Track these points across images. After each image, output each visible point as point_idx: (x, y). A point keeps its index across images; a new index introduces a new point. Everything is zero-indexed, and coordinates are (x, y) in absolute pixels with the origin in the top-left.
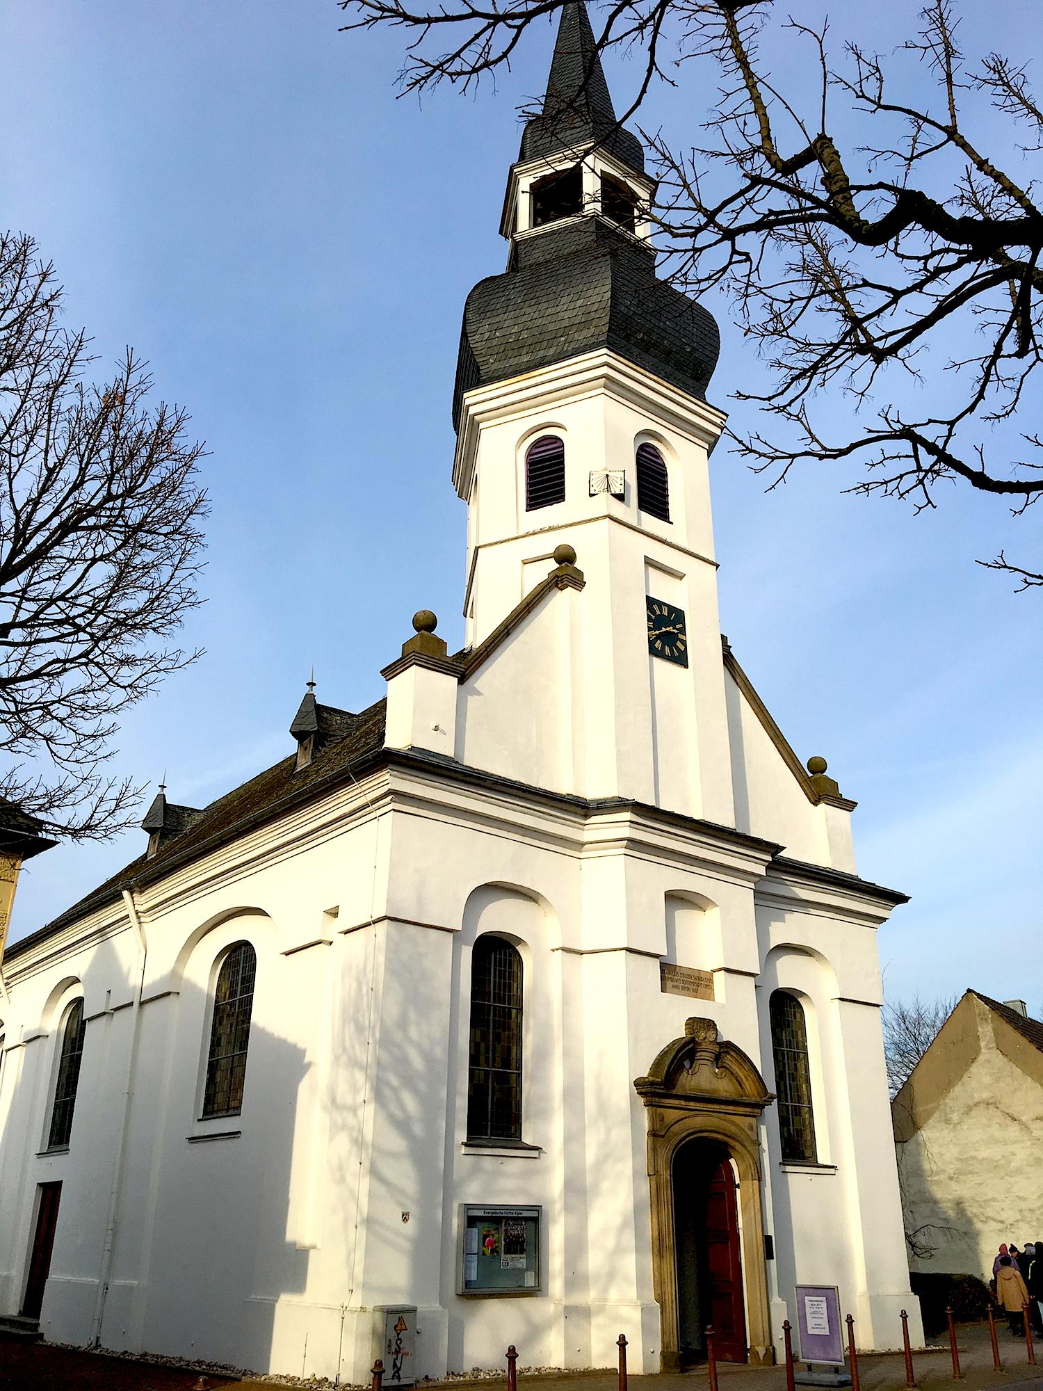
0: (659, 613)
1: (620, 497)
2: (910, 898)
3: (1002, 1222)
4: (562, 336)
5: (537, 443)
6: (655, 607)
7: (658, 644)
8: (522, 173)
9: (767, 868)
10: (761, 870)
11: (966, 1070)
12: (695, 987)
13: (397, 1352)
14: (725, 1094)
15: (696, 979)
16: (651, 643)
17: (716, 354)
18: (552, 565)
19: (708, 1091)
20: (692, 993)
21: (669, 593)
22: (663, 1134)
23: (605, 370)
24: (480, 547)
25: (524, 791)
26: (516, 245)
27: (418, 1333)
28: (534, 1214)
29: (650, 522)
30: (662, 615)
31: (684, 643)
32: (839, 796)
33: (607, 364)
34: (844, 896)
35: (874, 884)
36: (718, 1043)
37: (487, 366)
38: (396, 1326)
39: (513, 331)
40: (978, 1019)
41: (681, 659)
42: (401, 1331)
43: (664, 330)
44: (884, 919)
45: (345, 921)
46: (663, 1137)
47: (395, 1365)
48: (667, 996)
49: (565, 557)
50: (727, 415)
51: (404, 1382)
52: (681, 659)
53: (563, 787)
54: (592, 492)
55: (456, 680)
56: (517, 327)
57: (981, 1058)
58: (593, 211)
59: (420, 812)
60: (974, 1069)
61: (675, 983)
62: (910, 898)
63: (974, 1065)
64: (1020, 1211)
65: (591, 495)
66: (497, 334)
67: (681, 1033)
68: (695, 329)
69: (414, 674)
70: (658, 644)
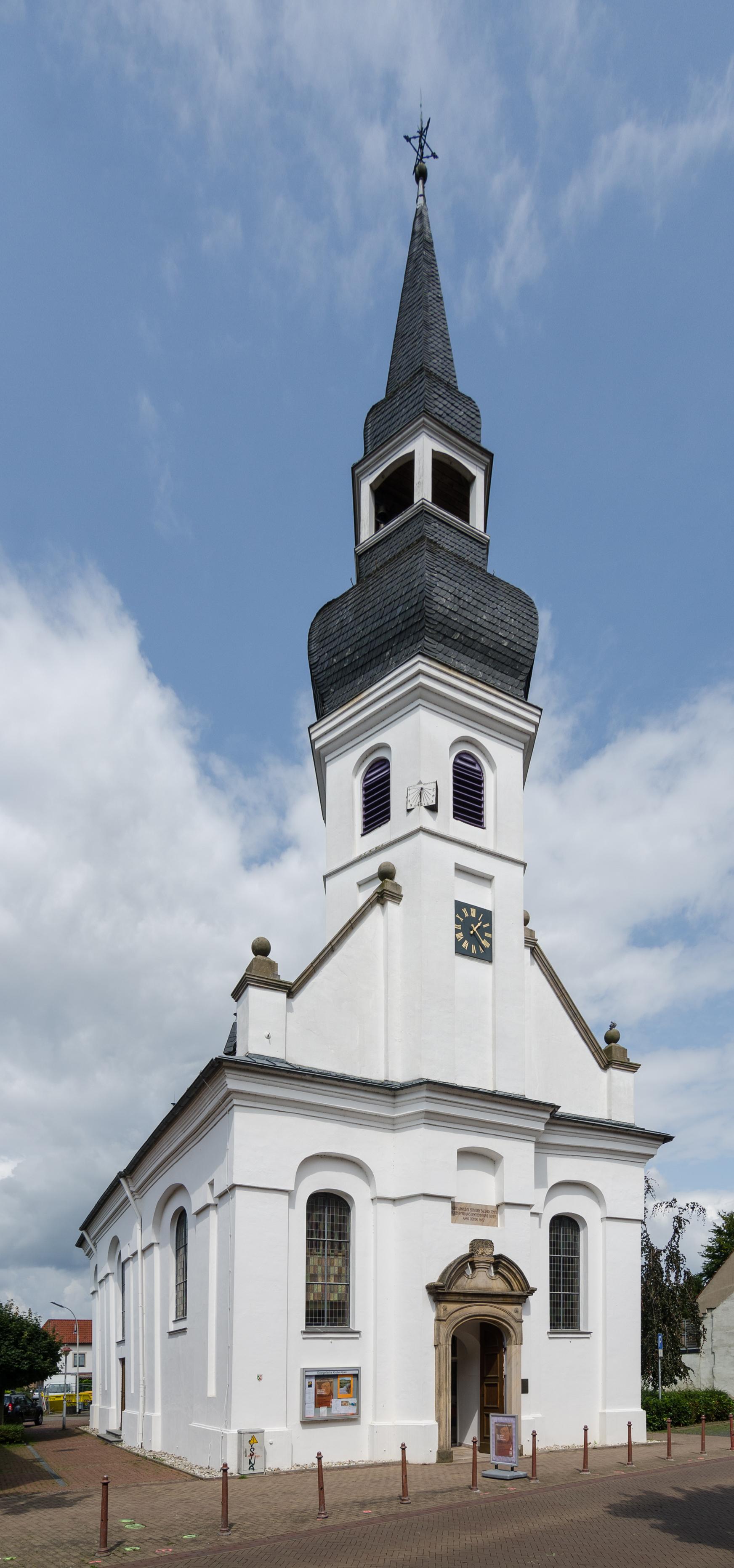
0: (468, 916)
1: (433, 809)
2: (674, 1137)
4: (386, 651)
5: (370, 768)
6: (464, 910)
7: (465, 945)
9: (547, 1124)
10: (541, 1127)
12: (482, 1218)
13: (252, 1455)
14: (497, 1290)
15: (483, 1212)
17: (533, 645)
19: (484, 1289)
22: (445, 1318)
23: (422, 680)
25: (339, 1080)
27: (271, 1444)
28: (356, 1372)
29: (463, 830)
31: (490, 940)
32: (627, 1061)
33: (420, 673)
35: (644, 1129)
36: (493, 1256)
37: (330, 696)
38: (250, 1441)
39: (347, 654)
41: (486, 956)
42: (253, 1443)
43: (480, 626)
44: (652, 1156)
46: (445, 1321)
47: (250, 1462)
48: (456, 1225)
49: (386, 874)
50: (541, 710)
52: (486, 956)
53: (378, 1076)
55: (285, 995)
56: (349, 649)
58: (421, 501)
59: (258, 1105)
61: (465, 1216)
62: (674, 1137)
66: (335, 660)
67: (466, 1251)
68: (513, 620)
69: (253, 993)
70: (465, 945)
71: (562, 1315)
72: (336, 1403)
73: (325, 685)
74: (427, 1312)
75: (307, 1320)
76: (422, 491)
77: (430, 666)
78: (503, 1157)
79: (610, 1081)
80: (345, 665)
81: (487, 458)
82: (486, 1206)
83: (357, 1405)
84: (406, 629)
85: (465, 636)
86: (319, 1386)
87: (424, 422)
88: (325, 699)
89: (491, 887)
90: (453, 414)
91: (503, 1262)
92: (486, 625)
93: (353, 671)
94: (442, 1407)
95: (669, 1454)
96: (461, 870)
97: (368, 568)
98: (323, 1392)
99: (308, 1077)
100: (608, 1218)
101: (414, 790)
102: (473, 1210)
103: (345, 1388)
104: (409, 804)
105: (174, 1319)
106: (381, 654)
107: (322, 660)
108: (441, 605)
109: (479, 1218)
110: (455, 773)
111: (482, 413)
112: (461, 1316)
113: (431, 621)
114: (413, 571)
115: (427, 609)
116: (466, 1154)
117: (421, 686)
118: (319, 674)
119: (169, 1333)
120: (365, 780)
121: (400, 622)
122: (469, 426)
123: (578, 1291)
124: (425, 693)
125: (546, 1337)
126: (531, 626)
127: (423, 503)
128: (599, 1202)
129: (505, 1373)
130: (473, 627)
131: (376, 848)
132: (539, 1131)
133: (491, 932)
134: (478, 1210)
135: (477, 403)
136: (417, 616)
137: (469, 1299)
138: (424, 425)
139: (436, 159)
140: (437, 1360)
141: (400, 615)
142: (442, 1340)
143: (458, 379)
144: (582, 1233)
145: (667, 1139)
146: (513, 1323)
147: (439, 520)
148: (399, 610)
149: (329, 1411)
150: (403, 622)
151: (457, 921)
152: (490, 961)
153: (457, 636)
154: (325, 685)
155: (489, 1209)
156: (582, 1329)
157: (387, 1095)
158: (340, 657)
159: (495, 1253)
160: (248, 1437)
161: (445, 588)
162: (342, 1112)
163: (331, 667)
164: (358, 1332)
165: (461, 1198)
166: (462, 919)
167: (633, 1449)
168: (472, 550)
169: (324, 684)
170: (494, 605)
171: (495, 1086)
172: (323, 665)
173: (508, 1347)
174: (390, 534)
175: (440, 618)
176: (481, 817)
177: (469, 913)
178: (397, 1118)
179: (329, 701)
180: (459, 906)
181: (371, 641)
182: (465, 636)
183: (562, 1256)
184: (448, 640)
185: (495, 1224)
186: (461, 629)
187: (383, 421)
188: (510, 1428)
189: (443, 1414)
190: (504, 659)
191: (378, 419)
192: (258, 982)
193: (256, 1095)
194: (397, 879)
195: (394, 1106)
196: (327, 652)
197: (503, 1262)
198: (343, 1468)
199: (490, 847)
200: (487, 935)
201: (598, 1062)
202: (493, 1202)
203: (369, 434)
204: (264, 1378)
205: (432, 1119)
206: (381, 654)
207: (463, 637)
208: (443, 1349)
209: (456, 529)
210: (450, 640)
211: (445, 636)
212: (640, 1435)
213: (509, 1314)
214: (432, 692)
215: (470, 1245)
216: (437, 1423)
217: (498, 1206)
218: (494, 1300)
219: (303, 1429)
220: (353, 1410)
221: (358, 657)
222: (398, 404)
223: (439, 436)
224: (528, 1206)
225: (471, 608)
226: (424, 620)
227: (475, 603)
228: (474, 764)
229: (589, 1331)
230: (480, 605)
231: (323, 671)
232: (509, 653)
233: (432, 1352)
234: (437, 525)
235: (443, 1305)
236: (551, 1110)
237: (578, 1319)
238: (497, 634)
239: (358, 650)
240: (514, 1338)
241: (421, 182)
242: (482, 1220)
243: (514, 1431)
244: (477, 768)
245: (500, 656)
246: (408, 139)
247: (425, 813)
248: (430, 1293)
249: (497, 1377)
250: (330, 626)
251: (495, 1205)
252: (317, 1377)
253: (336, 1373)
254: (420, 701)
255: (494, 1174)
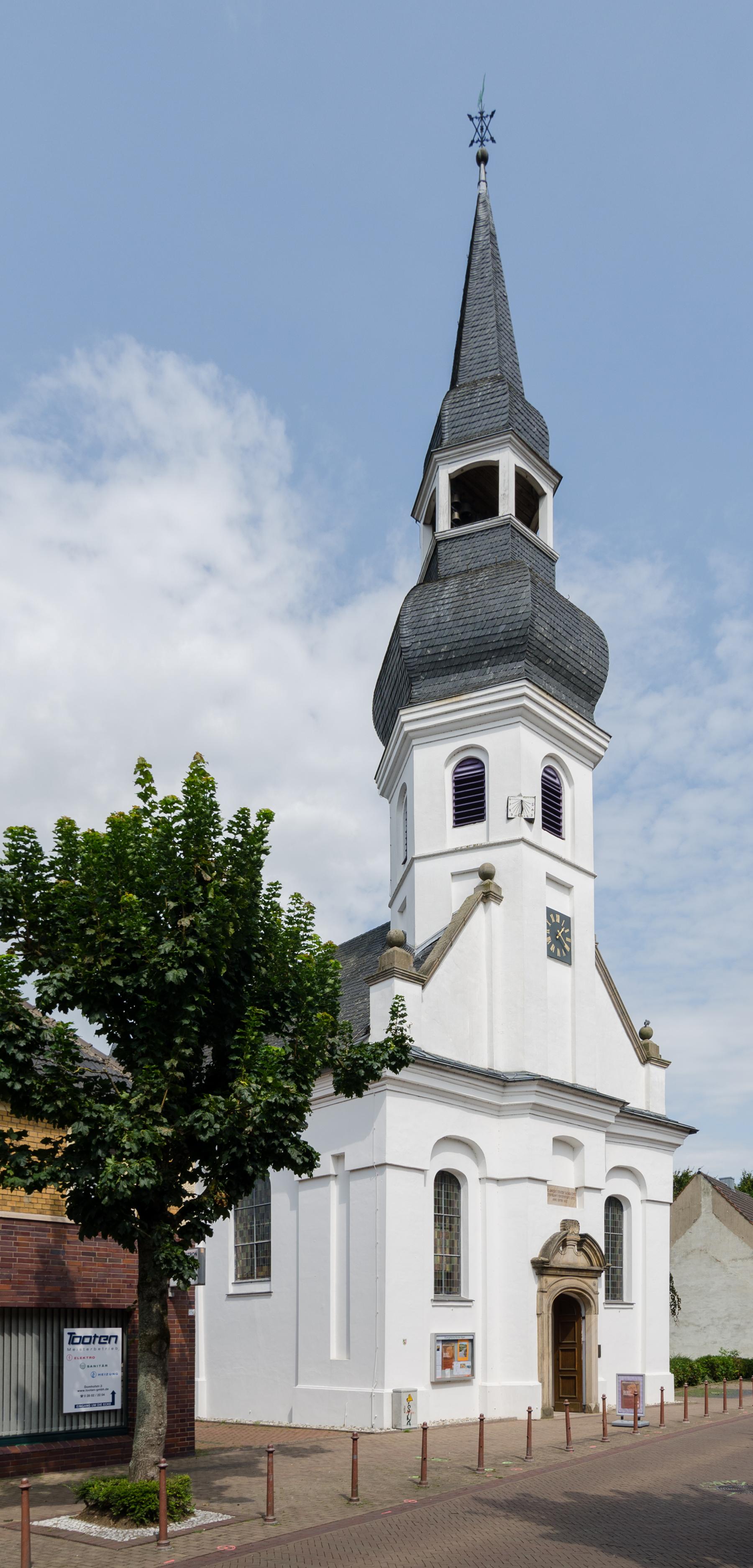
1: (530, 821)
3: (699, 1326)
4: (485, 660)
6: (552, 916)
7: (553, 948)
8: (442, 460)
11: (689, 1228)
13: (409, 1412)
16: (549, 946)
18: (477, 881)
20: (563, 1203)
21: (562, 904)
24: (416, 858)
26: (437, 543)
28: (471, 1338)
29: (547, 839)
30: (556, 922)
31: (569, 944)
33: (524, 695)
34: (656, 1131)
40: (702, 1192)
44: (680, 1145)
45: (350, 1163)
49: (486, 875)
50: (611, 737)
51: (412, 1426)
52: (566, 958)
53: (482, 1063)
54: (510, 816)
57: (700, 1220)
58: (509, 516)
60: (694, 1227)
63: (695, 1224)
64: (712, 1319)
65: (509, 819)
71: (443, 1279)
72: (456, 1365)
73: (415, 671)
74: (531, 1283)
75: (435, 1289)
76: (508, 504)
77: (533, 691)
78: (582, 1145)
79: (648, 1075)
80: (440, 659)
81: (557, 477)
82: (568, 1188)
83: (472, 1367)
84: (507, 647)
85: (555, 662)
86: (445, 1350)
87: (510, 438)
88: (413, 684)
89: (569, 894)
90: (528, 430)
91: (588, 1241)
92: (572, 654)
93: (447, 667)
94: (545, 1369)
95: (725, 1408)
96: (551, 879)
97: (447, 557)
98: (447, 1355)
99: (447, 1068)
100: (648, 1201)
101: (514, 801)
102: (559, 1192)
103: (463, 1352)
104: (509, 813)
105: (233, 1281)
106: (479, 661)
107: (416, 647)
108: (540, 634)
109: (564, 1199)
110: (543, 786)
111: (549, 430)
112: (557, 1288)
113: (531, 646)
114: (517, 597)
115: (529, 636)
116: (559, 1141)
117: (524, 707)
118: (409, 658)
119: (228, 1295)
120: (455, 773)
121: (502, 639)
122: (540, 442)
123: (622, 1265)
124: (525, 713)
125: (431, 1304)
126: (604, 658)
127: (510, 518)
128: (639, 1186)
129: (583, 1339)
130: (562, 655)
131: (474, 845)
132: (610, 1123)
133: (570, 937)
134: (563, 1192)
135: (545, 419)
136: (520, 639)
137: (563, 1273)
138: (510, 441)
139: (494, 144)
140: (540, 1327)
141: (502, 632)
142: (545, 1310)
143: (524, 385)
144: (625, 1213)
145: (692, 1131)
146: (592, 1294)
147: (521, 534)
148: (502, 628)
149: (452, 1373)
150: (505, 640)
151: (548, 927)
152: (570, 964)
153: (549, 661)
154: (415, 671)
155: (570, 1191)
156: (625, 1300)
157: (499, 1085)
158: (435, 650)
159: (581, 1232)
160: (405, 1397)
161: (544, 618)
162: (465, 1099)
163: (424, 656)
164: (471, 1301)
165: (555, 1182)
166: (550, 924)
167: (665, 1408)
168: (545, 566)
169: (414, 670)
170: (577, 637)
171: (575, 1079)
172: (415, 652)
173: (587, 1317)
174: (473, 533)
175: (539, 645)
176: (560, 827)
177: (555, 919)
178: (504, 1106)
179: (419, 686)
180: (550, 912)
181: (470, 647)
182: (555, 662)
183: (610, 1233)
184: (542, 664)
185: (574, 1205)
186: (553, 656)
187: (462, 415)
188: (637, 1385)
189: (546, 1375)
190: (582, 686)
191: (457, 410)
192: (403, 975)
193: (404, 1082)
194: (496, 880)
195: (503, 1094)
196: (421, 641)
197: (588, 1241)
198: (461, 1425)
199: (568, 858)
200: (567, 939)
201: (638, 1057)
202: (573, 1186)
203: (446, 421)
204: (408, 1342)
205: (538, 1110)
206: (479, 661)
207: (553, 663)
208: (545, 1317)
209: (533, 544)
210: (543, 664)
211: (540, 661)
212: (670, 1397)
213: (589, 1286)
214: (531, 712)
215: (562, 1224)
216: (541, 1384)
217: (577, 1189)
218: (581, 1274)
219: (433, 1389)
220: (468, 1372)
221: (454, 656)
222: (479, 405)
223: (521, 453)
224: (545, 1181)
225: (562, 639)
226: (526, 645)
227: (564, 634)
228: (555, 778)
229: (470, 1298)
230: (568, 637)
231: (414, 658)
232: (586, 681)
233: (535, 1319)
234: (519, 539)
235: (545, 1277)
236: (621, 1105)
237: (458, 1283)
238: (579, 663)
239: (455, 650)
240: (593, 1309)
241: (482, 165)
242: (566, 1201)
243: (641, 1387)
244: (557, 781)
245: (580, 682)
246: (471, 119)
247: (524, 823)
248: (534, 1268)
249: (575, 1343)
250: (424, 617)
251: (574, 1187)
252: (444, 1341)
253: (455, 1338)
254: (520, 719)
255: (573, 1160)
